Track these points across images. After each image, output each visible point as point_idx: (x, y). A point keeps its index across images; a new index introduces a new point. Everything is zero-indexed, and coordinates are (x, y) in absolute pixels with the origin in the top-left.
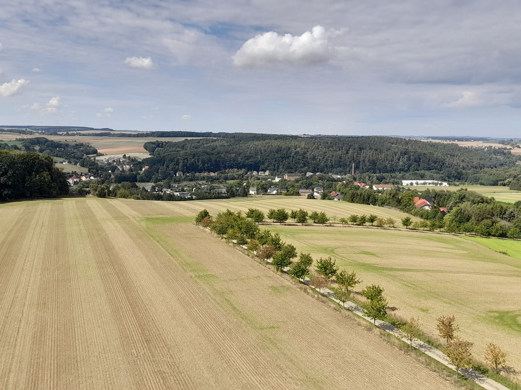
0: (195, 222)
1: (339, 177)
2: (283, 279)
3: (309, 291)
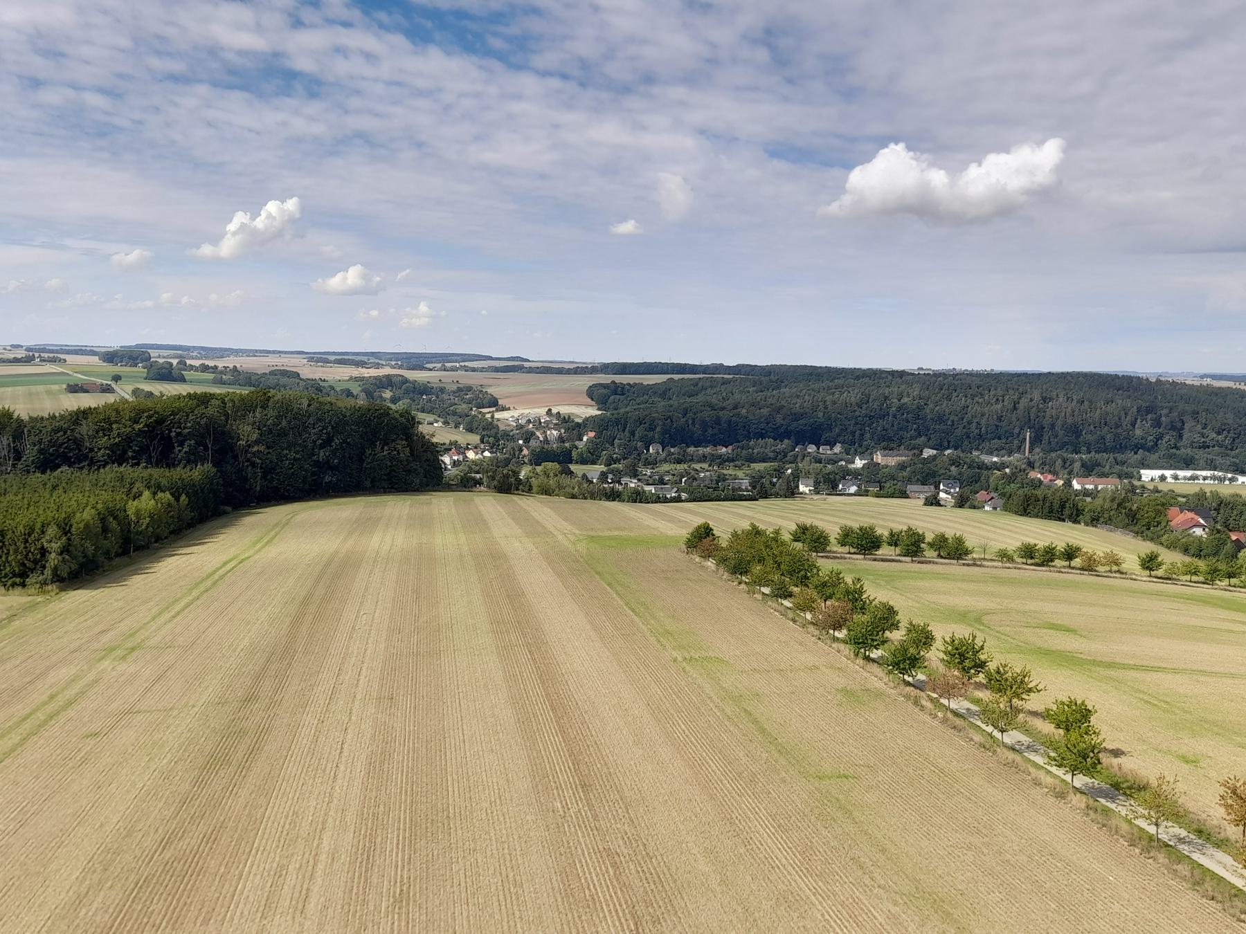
0: (684, 547)
1: (995, 459)
2: (868, 674)
3: (924, 703)
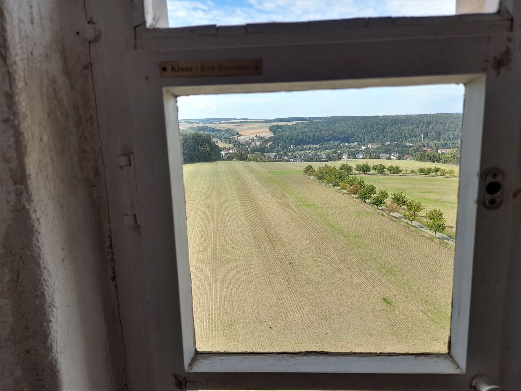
0: (303, 173)
1: (411, 144)
2: (366, 207)
3: (385, 214)
